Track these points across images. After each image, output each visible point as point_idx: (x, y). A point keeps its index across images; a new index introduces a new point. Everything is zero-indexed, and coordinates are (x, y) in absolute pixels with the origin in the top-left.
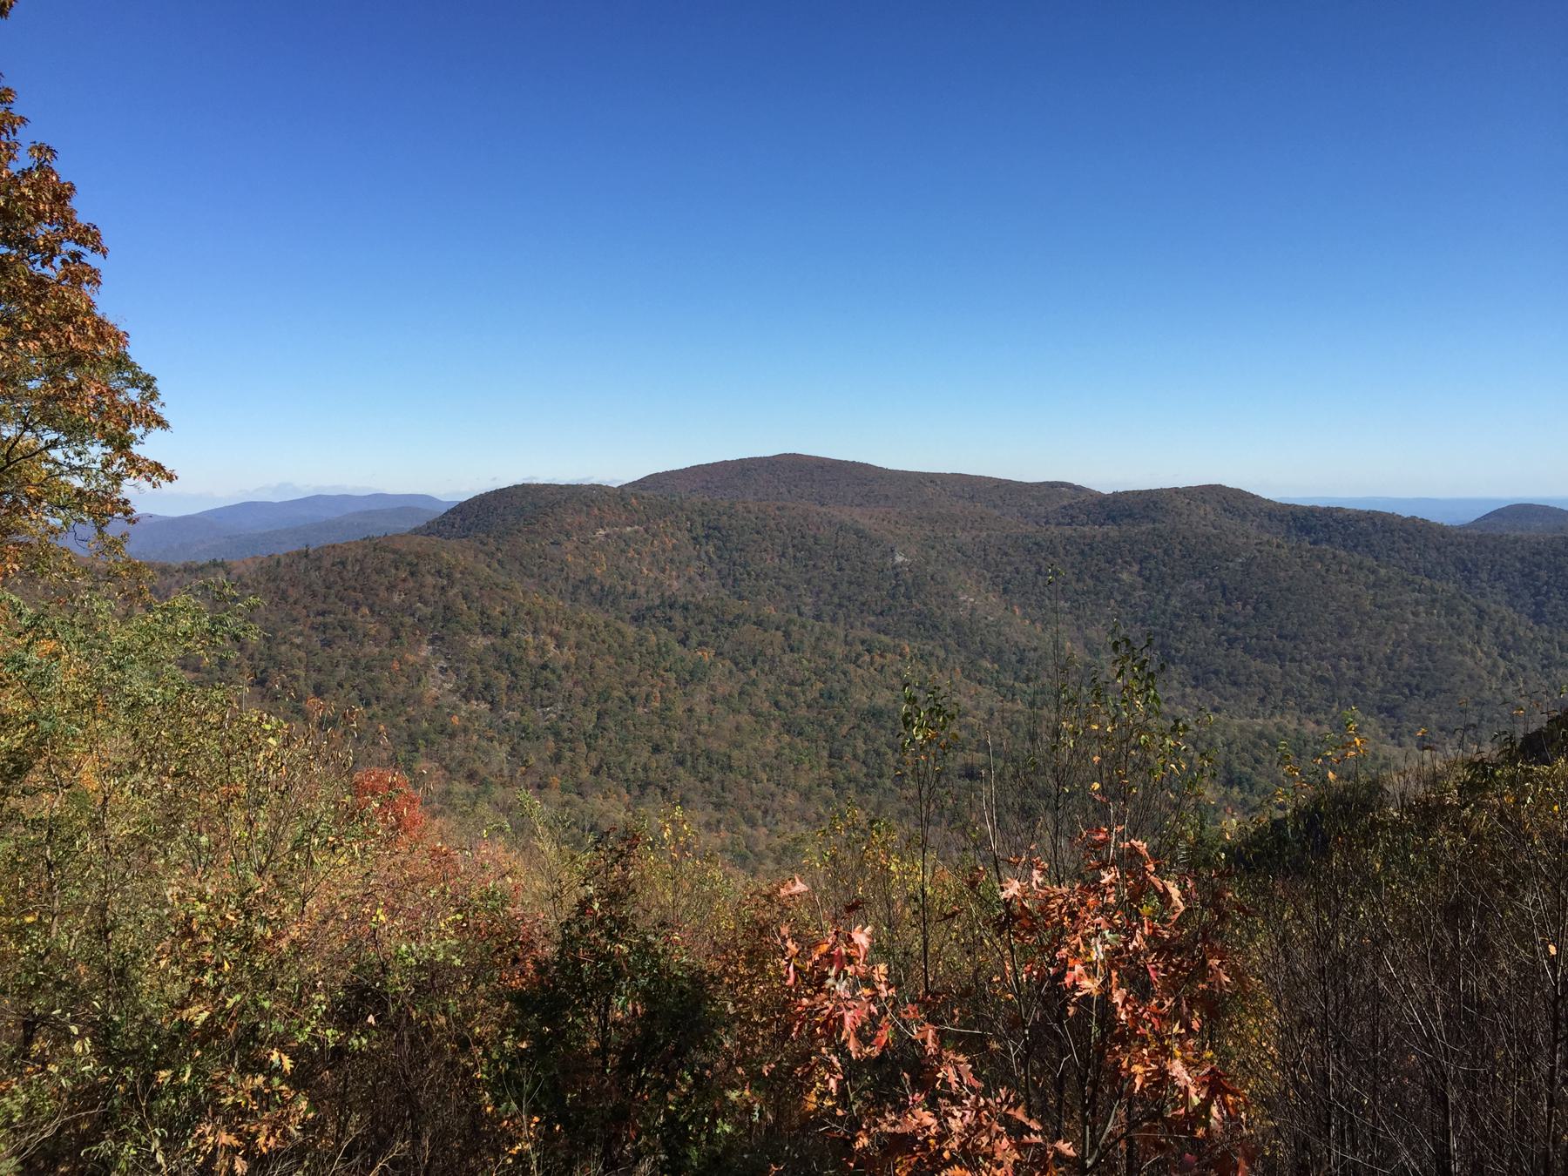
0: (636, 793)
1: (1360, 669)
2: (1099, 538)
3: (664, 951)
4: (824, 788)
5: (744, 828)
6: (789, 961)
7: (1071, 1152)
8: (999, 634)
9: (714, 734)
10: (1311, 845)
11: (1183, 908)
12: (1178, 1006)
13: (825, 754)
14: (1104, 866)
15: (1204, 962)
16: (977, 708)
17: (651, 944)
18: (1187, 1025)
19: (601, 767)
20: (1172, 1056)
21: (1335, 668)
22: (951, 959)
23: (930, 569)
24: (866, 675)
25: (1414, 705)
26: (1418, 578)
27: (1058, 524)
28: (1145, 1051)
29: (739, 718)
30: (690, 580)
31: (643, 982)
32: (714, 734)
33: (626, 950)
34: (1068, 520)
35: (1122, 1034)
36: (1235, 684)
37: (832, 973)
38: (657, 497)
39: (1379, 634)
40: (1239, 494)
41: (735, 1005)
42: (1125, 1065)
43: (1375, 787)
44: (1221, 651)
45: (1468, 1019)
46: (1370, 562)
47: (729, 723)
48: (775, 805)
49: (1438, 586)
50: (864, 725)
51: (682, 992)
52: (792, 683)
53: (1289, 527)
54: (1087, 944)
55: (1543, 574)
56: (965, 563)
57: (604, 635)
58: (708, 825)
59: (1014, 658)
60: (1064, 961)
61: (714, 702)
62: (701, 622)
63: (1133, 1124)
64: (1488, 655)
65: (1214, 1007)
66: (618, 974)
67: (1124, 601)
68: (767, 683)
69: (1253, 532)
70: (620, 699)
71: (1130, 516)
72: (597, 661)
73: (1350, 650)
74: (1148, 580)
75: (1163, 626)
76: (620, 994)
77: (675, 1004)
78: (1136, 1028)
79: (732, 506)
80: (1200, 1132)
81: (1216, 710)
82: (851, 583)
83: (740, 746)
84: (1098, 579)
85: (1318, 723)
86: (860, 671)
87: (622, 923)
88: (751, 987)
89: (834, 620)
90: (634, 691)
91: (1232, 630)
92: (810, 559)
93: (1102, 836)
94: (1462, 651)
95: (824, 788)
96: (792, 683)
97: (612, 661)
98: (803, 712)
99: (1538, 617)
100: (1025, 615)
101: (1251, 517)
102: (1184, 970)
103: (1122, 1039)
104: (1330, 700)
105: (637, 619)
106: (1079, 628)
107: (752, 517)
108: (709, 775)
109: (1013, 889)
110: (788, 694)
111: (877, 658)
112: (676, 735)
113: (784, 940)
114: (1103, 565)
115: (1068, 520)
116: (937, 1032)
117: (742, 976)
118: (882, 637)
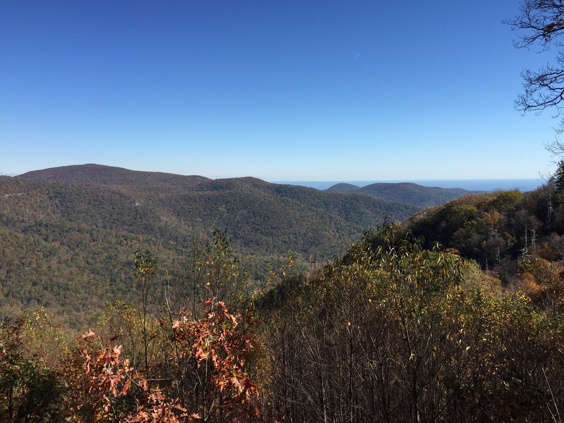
0: (26, 302)
1: (296, 238)
2: (211, 195)
3: (36, 366)
4: (108, 294)
5: (75, 312)
6: (87, 363)
7: (198, 417)
8: (176, 231)
9: (60, 276)
10: (279, 299)
11: (237, 324)
12: (236, 359)
13: (109, 280)
14: (210, 312)
15: (244, 342)
16: (169, 258)
17: (30, 364)
18: (239, 365)
19: (9, 293)
20: (233, 377)
21: (289, 238)
22: (156, 353)
23: (149, 208)
24: (125, 249)
25: (312, 248)
26: (313, 207)
27: (197, 191)
28: (224, 376)
29: (71, 269)
30: (48, 214)
31: (27, 380)
32: (60, 276)
33: (18, 367)
34: (200, 189)
35: (216, 371)
36: (258, 245)
37: (105, 365)
38: (32, 181)
39: (302, 226)
40: (258, 180)
41: (68, 384)
42: (217, 382)
43: (301, 277)
44: (253, 234)
45: (326, 350)
46: (298, 202)
47: (67, 272)
48: (88, 302)
49: (318, 210)
50: (124, 268)
51: (45, 381)
52: (94, 254)
53: (274, 191)
54: (204, 341)
55: (348, 205)
56: (163, 205)
57: (9, 238)
58: (58, 313)
59: (182, 240)
60: (196, 349)
61: (60, 263)
62: (54, 231)
63: (221, 403)
64: (333, 231)
65: (249, 357)
66: (15, 377)
67: (220, 218)
68: (83, 254)
69: (262, 193)
70: (17, 264)
71: (222, 188)
72: (6, 249)
73: (293, 232)
74: (229, 210)
75: (234, 226)
76: (16, 386)
77: (42, 387)
78: (221, 369)
79: (66, 184)
80: (243, 401)
81: (252, 254)
82: (118, 214)
83: (70, 280)
84: (211, 210)
85: (284, 256)
86: (122, 248)
87: (16, 357)
88: (76, 375)
89: (111, 228)
90: (24, 261)
91: (257, 226)
92: (101, 205)
93: (209, 301)
94: (326, 230)
95: (108, 294)
96: (94, 254)
97: (13, 249)
98: (99, 265)
99: (347, 219)
100: (186, 224)
101: (262, 188)
102: (238, 345)
103: (216, 373)
104: (288, 249)
105: (24, 231)
106: (205, 228)
107: (75, 189)
108: (58, 293)
109: (176, 324)
110: (92, 258)
111: (129, 242)
112: (44, 278)
113: (85, 355)
114: (213, 205)
115: (200, 189)
116: (148, 382)
117: (72, 372)
118: (131, 234)
